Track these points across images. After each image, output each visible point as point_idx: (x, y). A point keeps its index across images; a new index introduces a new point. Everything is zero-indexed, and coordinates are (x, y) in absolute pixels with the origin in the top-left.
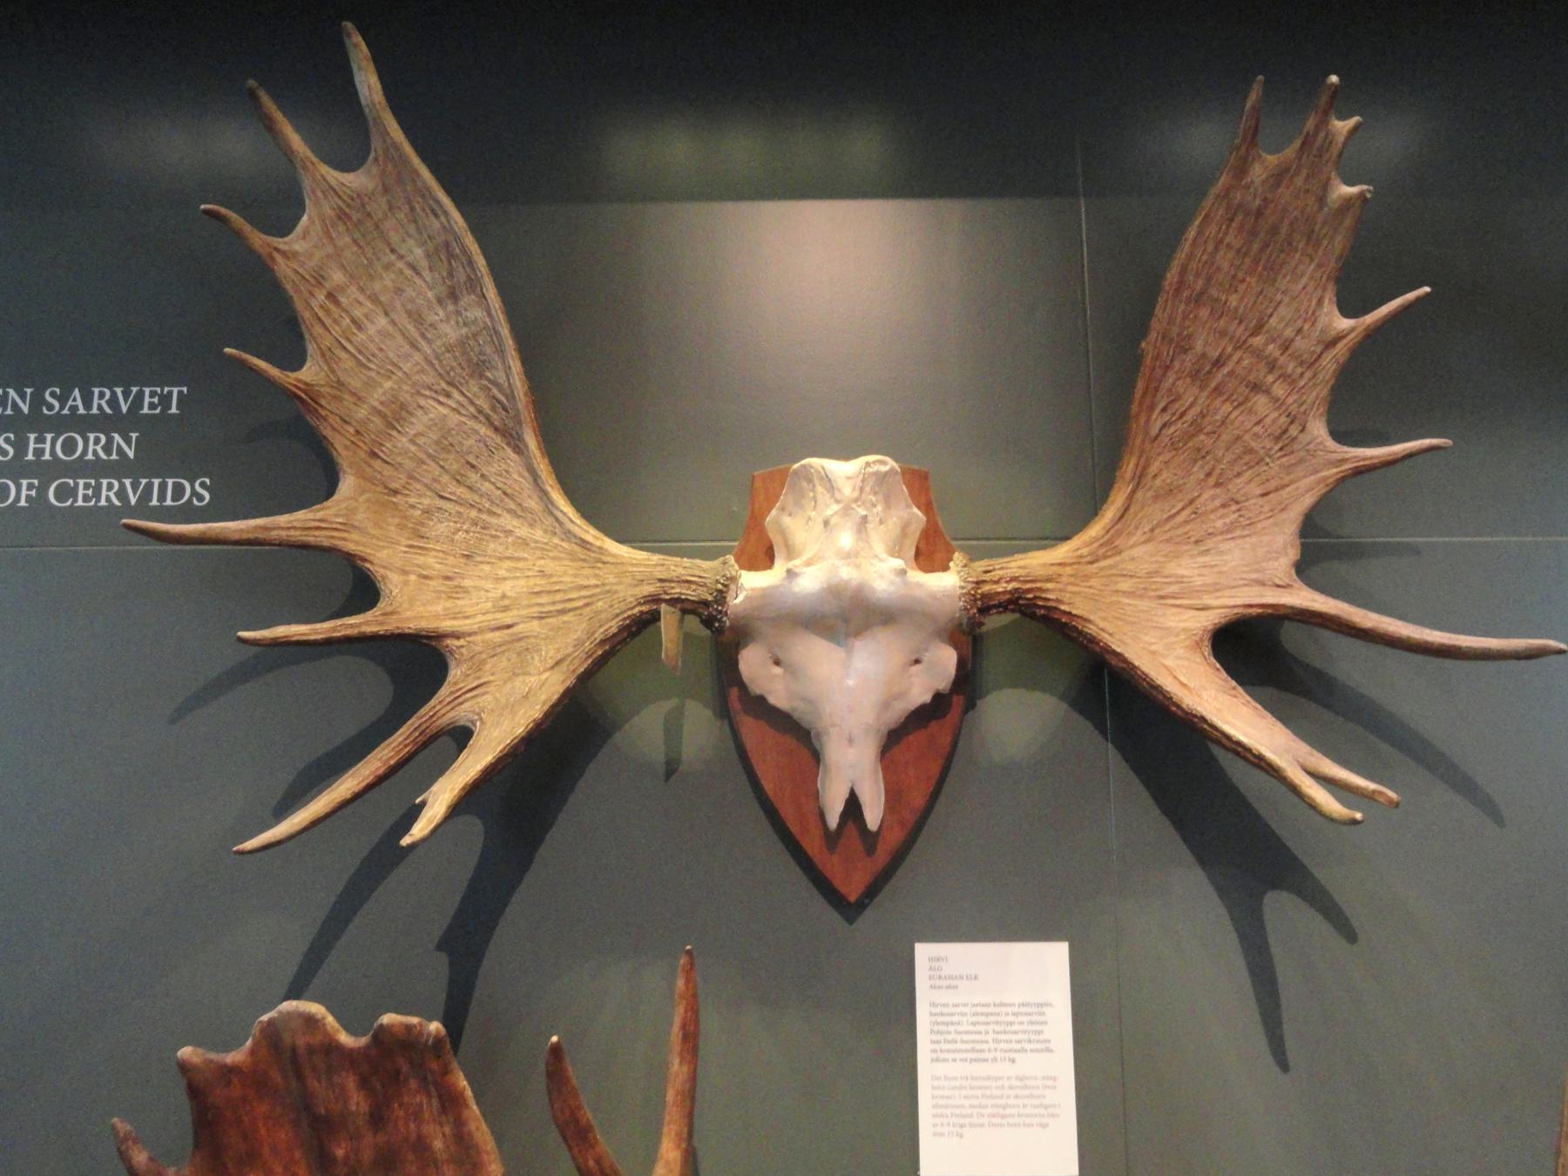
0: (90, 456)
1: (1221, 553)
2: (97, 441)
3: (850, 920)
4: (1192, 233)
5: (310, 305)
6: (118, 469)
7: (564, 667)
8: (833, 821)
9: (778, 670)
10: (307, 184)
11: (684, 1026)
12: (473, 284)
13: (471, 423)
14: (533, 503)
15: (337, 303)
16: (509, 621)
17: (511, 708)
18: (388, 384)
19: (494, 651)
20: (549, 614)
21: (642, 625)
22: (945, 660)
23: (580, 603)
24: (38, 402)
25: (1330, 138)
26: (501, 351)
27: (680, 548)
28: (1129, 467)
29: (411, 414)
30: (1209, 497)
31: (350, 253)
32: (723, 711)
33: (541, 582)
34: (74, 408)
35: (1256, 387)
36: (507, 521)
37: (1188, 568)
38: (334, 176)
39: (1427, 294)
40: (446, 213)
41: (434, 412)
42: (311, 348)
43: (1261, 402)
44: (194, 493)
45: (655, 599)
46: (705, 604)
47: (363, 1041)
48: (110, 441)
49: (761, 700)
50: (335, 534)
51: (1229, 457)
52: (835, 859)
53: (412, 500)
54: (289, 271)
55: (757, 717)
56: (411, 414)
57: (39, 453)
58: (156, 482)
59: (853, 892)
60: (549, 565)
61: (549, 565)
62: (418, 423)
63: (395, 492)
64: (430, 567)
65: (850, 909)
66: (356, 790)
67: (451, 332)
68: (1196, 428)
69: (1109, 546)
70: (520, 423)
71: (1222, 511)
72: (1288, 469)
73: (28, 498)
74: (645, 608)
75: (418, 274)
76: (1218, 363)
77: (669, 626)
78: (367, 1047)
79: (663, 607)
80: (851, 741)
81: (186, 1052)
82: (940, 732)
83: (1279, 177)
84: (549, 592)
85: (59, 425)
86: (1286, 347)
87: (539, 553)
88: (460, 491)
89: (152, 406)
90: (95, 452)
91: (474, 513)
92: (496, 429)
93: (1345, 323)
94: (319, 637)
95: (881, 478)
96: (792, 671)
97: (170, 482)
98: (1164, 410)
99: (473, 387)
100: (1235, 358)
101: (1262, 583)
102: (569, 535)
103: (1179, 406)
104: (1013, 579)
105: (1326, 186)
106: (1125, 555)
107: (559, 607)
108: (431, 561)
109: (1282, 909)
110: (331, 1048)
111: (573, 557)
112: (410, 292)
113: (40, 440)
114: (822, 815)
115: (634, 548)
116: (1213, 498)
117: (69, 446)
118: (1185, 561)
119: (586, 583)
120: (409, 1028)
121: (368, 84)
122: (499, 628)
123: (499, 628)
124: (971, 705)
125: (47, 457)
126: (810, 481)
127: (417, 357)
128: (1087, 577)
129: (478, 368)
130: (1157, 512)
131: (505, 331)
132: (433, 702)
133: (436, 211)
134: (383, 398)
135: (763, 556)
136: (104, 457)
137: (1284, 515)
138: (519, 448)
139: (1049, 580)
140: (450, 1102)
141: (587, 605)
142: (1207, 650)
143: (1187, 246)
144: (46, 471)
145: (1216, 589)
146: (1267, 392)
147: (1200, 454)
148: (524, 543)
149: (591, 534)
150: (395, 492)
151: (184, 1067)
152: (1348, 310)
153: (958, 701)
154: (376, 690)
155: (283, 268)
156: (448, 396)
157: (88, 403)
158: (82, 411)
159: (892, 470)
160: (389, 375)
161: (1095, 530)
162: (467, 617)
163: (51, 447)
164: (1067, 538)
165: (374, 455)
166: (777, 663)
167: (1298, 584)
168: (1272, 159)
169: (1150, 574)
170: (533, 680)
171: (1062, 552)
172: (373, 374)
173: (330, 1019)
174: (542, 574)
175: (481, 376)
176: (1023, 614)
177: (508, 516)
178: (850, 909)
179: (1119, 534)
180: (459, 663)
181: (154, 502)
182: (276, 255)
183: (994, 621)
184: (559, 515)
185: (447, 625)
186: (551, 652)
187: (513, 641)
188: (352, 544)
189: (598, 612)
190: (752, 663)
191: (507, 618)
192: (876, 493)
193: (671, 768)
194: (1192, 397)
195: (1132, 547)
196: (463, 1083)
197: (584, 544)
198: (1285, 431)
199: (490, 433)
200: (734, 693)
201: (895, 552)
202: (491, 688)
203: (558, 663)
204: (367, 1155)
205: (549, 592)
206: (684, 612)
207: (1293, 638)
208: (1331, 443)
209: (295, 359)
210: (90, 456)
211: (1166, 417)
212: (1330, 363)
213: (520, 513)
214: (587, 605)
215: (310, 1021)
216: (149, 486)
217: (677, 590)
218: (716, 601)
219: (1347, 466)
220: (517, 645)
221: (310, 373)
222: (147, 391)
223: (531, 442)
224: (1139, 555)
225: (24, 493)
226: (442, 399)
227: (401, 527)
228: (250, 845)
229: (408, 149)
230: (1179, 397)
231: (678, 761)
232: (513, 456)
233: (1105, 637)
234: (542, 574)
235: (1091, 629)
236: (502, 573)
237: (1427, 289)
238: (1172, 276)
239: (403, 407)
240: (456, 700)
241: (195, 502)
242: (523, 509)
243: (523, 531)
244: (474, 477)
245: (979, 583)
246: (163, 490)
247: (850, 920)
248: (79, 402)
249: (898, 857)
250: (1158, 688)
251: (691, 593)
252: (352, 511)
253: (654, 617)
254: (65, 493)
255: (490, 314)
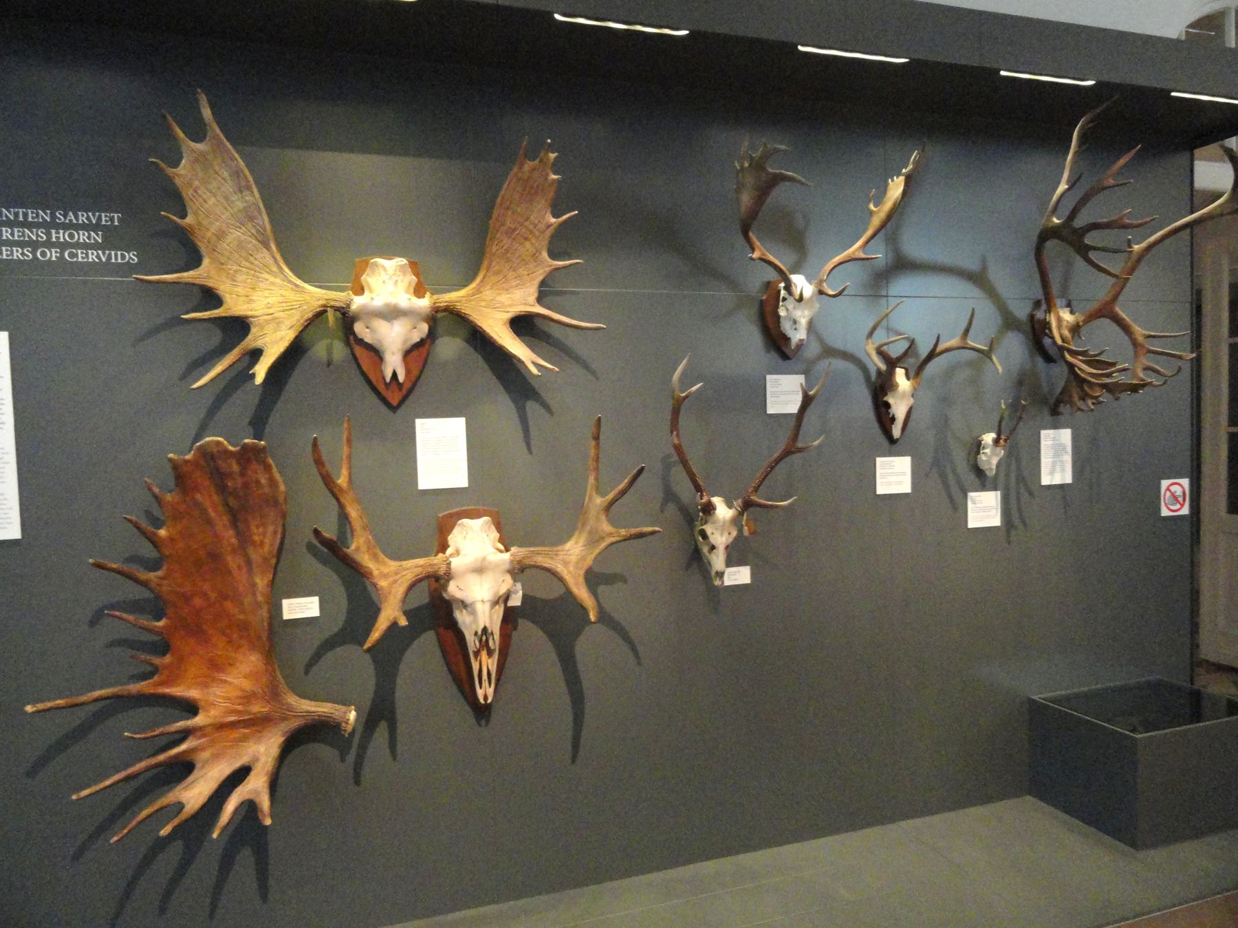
0: (81, 241)
1: (513, 294)
2: (84, 234)
3: (394, 412)
4: (505, 186)
5: (187, 194)
6: (96, 246)
7: (293, 329)
8: (388, 379)
9: (368, 330)
10: (184, 148)
11: (347, 438)
12: (249, 188)
13: (250, 239)
14: (275, 269)
15: (197, 193)
16: (271, 312)
17: (276, 342)
18: (218, 224)
19: (267, 322)
20: (286, 310)
21: (320, 315)
22: (424, 328)
23: (297, 306)
24: (53, 216)
25: (548, 159)
26: (260, 214)
27: (325, 286)
28: (485, 263)
29: (227, 235)
30: (511, 274)
31: (201, 174)
32: (348, 343)
33: (281, 299)
34: (71, 220)
35: (526, 239)
36: (266, 276)
37: (504, 298)
38: (192, 144)
39: (576, 215)
40: (236, 160)
41: (235, 235)
42: (189, 211)
43: (528, 245)
44: (130, 258)
45: (324, 306)
46: (343, 308)
47: (238, 448)
48: (89, 235)
49: (362, 340)
50: (205, 280)
51: (518, 261)
52: (390, 392)
53: (229, 267)
54: (180, 183)
55: (360, 345)
56: (227, 235)
57: (58, 238)
58: (113, 253)
59: (395, 403)
60: (284, 293)
61: (284, 293)
62: (230, 238)
63: (223, 264)
64: (240, 292)
65: (394, 409)
66: (224, 369)
67: (240, 205)
68: (507, 251)
69: (478, 291)
70: (269, 240)
71: (515, 280)
72: (536, 266)
73: (56, 257)
74: (322, 309)
75: (226, 181)
76: (514, 230)
77: (331, 315)
78: (240, 450)
79: (329, 309)
80: (393, 354)
81: (171, 455)
82: (424, 350)
83: (534, 169)
84: (286, 302)
85: (65, 227)
86: (535, 226)
87: (279, 288)
88: (247, 264)
89: (106, 221)
90: (84, 239)
91: (253, 272)
92: (259, 241)
93: (553, 220)
94: (206, 317)
95: (402, 267)
96: (373, 331)
97: (119, 253)
98: (497, 245)
99: (250, 225)
100: (519, 229)
101: (525, 304)
102: (290, 282)
103: (501, 244)
104: (446, 302)
105: (547, 175)
106: (484, 293)
107: (290, 307)
108: (240, 290)
109: (531, 406)
110: (226, 451)
111: (292, 289)
112: (223, 189)
113: (57, 233)
114: (384, 378)
115: (311, 285)
116: (512, 275)
117: (71, 236)
118: (503, 296)
119: (298, 299)
120: (254, 443)
121: (207, 113)
122: (267, 315)
123: (267, 315)
124: (433, 342)
125: (62, 240)
126: (377, 266)
127: (228, 214)
128: (470, 301)
129: (252, 219)
130: (494, 279)
131: (261, 206)
132: (246, 340)
133: (232, 159)
134: (217, 229)
135: (360, 290)
136: (87, 241)
137: (533, 282)
138: (268, 248)
139: (457, 302)
140: (268, 468)
141: (299, 307)
142: (508, 325)
143: (504, 190)
144: (63, 246)
145: (511, 306)
146: (529, 241)
147: (508, 260)
148: (273, 284)
149: (299, 282)
150: (223, 264)
151: (170, 460)
152: (555, 216)
153: (428, 341)
154: (217, 337)
155: (178, 181)
156: (240, 228)
157: (77, 218)
158: (75, 221)
159: (406, 264)
160: (217, 220)
161: (473, 285)
162: (256, 311)
163: (63, 236)
164: (465, 286)
165: (214, 250)
166: (368, 328)
167: (537, 305)
168: (531, 163)
169: (492, 300)
170: (283, 333)
171: (463, 292)
172: (212, 220)
173: (225, 442)
174: (282, 296)
175: (253, 221)
176: (450, 313)
177: (266, 274)
178: (394, 409)
179: (482, 286)
180: (255, 327)
181: (113, 261)
182: (176, 176)
183: (439, 315)
184: (286, 274)
185: (249, 313)
186: (288, 323)
187: (273, 319)
188: (210, 283)
189: (305, 310)
190: (358, 328)
191: (271, 311)
192: (400, 272)
193: (329, 364)
194: (506, 242)
195: (486, 291)
196: (271, 461)
197: (296, 286)
198: (535, 254)
199: (257, 243)
200: (351, 338)
201: (407, 292)
202: (268, 336)
203: (291, 327)
204: (239, 486)
205: (286, 302)
206: (335, 310)
207: (538, 322)
208: (549, 260)
209: (184, 216)
210: (81, 241)
211: (497, 248)
212: (548, 233)
213: (270, 272)
214: (299, 307)
215: (218, 443)
216: (110, 254)
217: (332, 303)
218: (347, 307)
219: (553, 267)
220: (277, 322)
221: (189, 220)
222: (103, 214)
223: (273, 247)
224: (488, 294)
225: (54, 255)
226: (239, 230)
227: (227, 277)
228: (195, 386)
229: (222, 136)
230: (502, 241)
231: (332, 361)
232: (267, 251)
233: (477, 321)
234: (282, 296)
235: (471, 318)
236: (267, 295)
237: (577, 212)
238: (499, 200)
239: (224, 232)
240: (255, 340)
241: (40, 239)
242: (272, 271)
243: (272, 279)
244: (252, 259)
245: (435, 303)
246: (117, 257)
247: (394, 412)
248: (73, 218)
249: (410, 391)
250: (492, 338)
251: (337, 304)
252: (209, 271)
253: (325, 311)
254: (72, 255)
255: (255, 199)
